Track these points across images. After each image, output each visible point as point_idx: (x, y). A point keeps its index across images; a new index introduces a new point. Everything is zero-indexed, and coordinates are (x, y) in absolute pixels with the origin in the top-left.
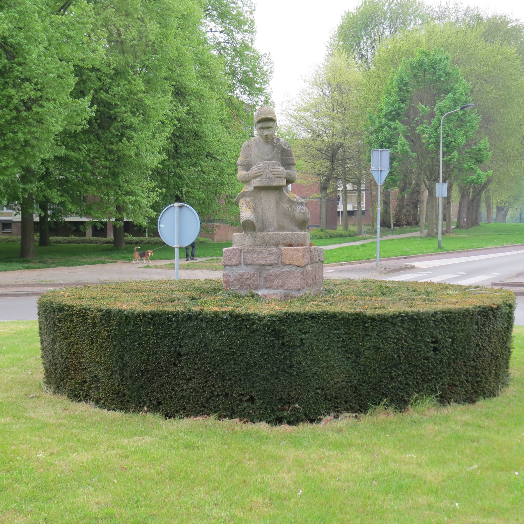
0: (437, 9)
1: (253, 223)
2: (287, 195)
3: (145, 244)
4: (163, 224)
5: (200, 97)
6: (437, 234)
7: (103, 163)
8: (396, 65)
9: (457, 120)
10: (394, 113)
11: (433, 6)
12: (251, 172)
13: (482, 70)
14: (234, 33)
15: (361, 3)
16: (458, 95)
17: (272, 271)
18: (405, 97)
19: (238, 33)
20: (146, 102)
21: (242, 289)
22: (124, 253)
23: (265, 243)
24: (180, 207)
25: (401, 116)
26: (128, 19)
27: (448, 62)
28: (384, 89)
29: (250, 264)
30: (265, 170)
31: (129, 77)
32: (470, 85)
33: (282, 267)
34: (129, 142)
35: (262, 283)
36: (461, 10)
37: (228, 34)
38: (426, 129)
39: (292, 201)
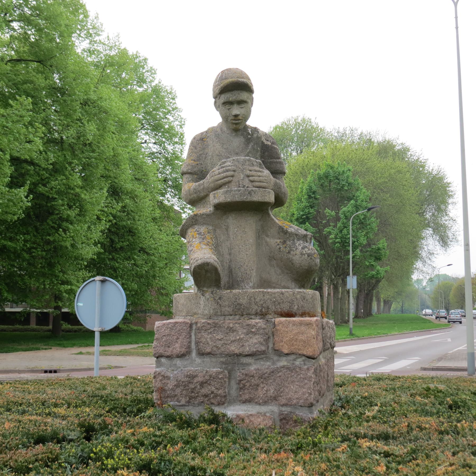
0: (336, 134)
1: (216, 269)
2: (277, 221)
3: (84, 332)
4: (81, 303)
5: (133, 197)
6: (348, 321)
7: (40, 253)
8: (305, 177)
9: (359, 224)
10: (305, 217)
11: (333, 132)
12: (208, 180)
13: (379, 181)
14: (166, 144)
15: (272, 129)
16: (359, 202)
17: (254, 367)
18: (314, 203)
19: (169, 144)
20: (83, 196)
21: (194, 405)
22: (61, 341)
23: (240, 311)
24: (103, 281)
25: (311, 220)
26: (68, 120)
27: (350, 174)
28: (295, 197)
29: (209, 354)
30: (236, 174)
31: (67, 173)
32: (369, 193)
33: (276, 358)
34: (65, 234)
35: (234, 392)
36: (356, 135)
37: (160, 145)
38: (333, 231)
39: (286, 232)
